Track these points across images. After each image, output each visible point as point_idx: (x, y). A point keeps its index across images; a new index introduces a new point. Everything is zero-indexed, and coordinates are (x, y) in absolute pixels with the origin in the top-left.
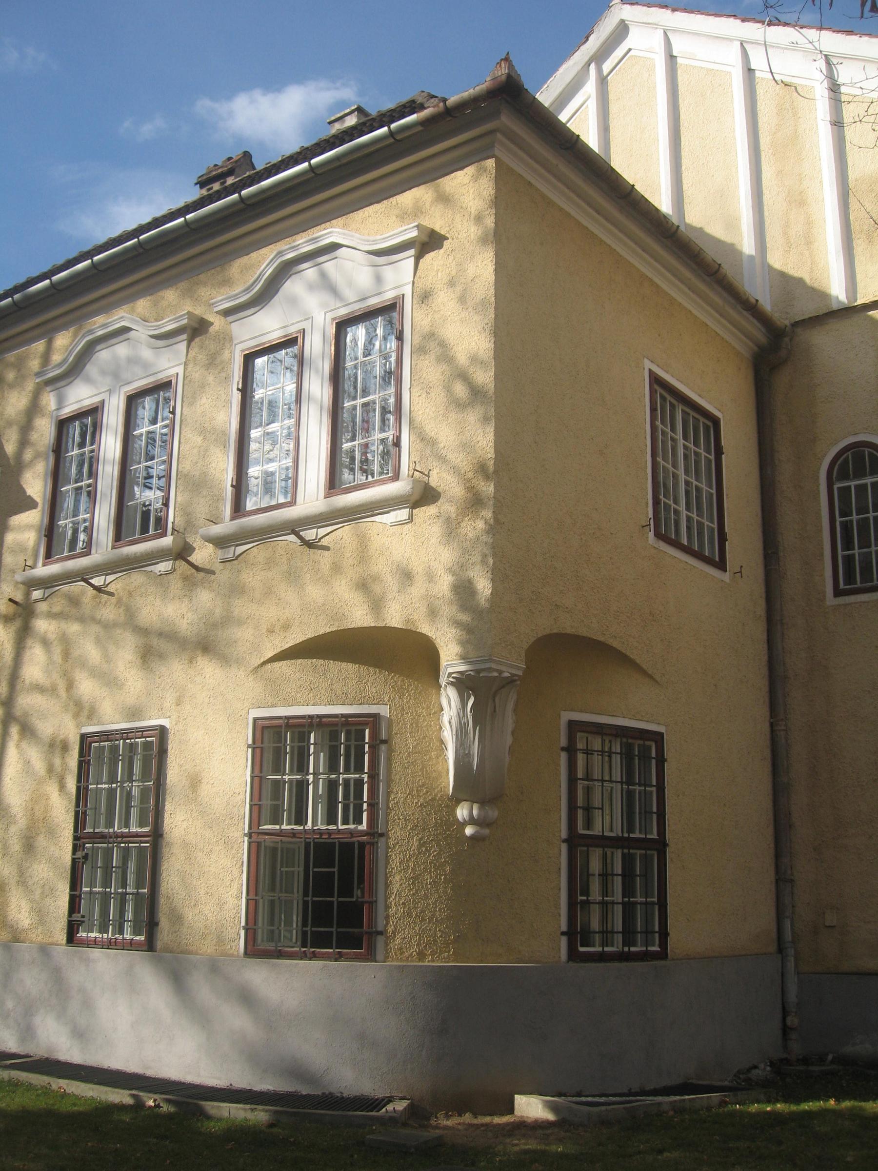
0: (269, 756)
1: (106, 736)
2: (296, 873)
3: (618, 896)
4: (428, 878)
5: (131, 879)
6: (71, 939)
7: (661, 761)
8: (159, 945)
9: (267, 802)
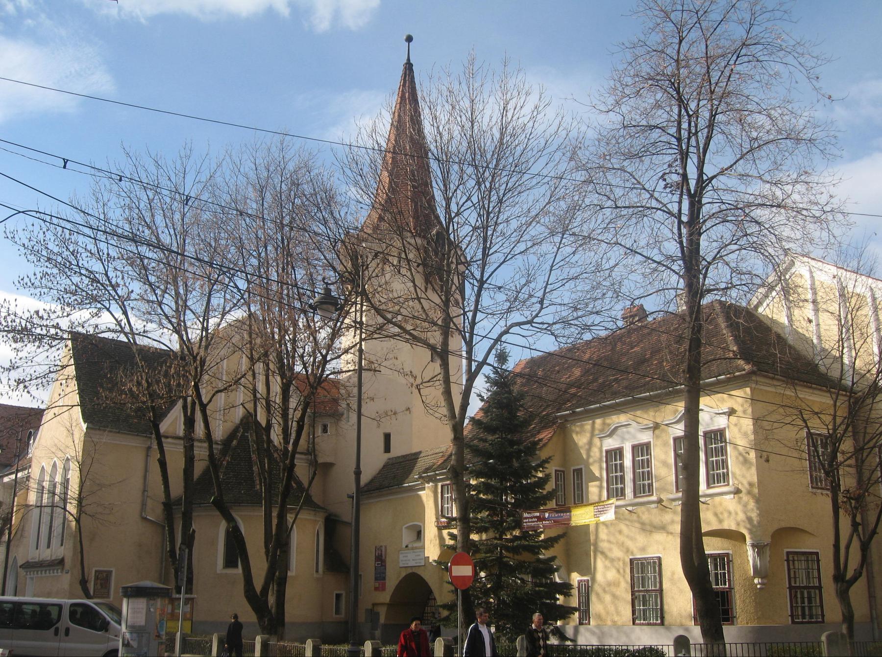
2: (55, 542)
3: (806, 604)
4: (748, 601)
6: (634, 623)
7: (818, 561)
8: (666, 623)
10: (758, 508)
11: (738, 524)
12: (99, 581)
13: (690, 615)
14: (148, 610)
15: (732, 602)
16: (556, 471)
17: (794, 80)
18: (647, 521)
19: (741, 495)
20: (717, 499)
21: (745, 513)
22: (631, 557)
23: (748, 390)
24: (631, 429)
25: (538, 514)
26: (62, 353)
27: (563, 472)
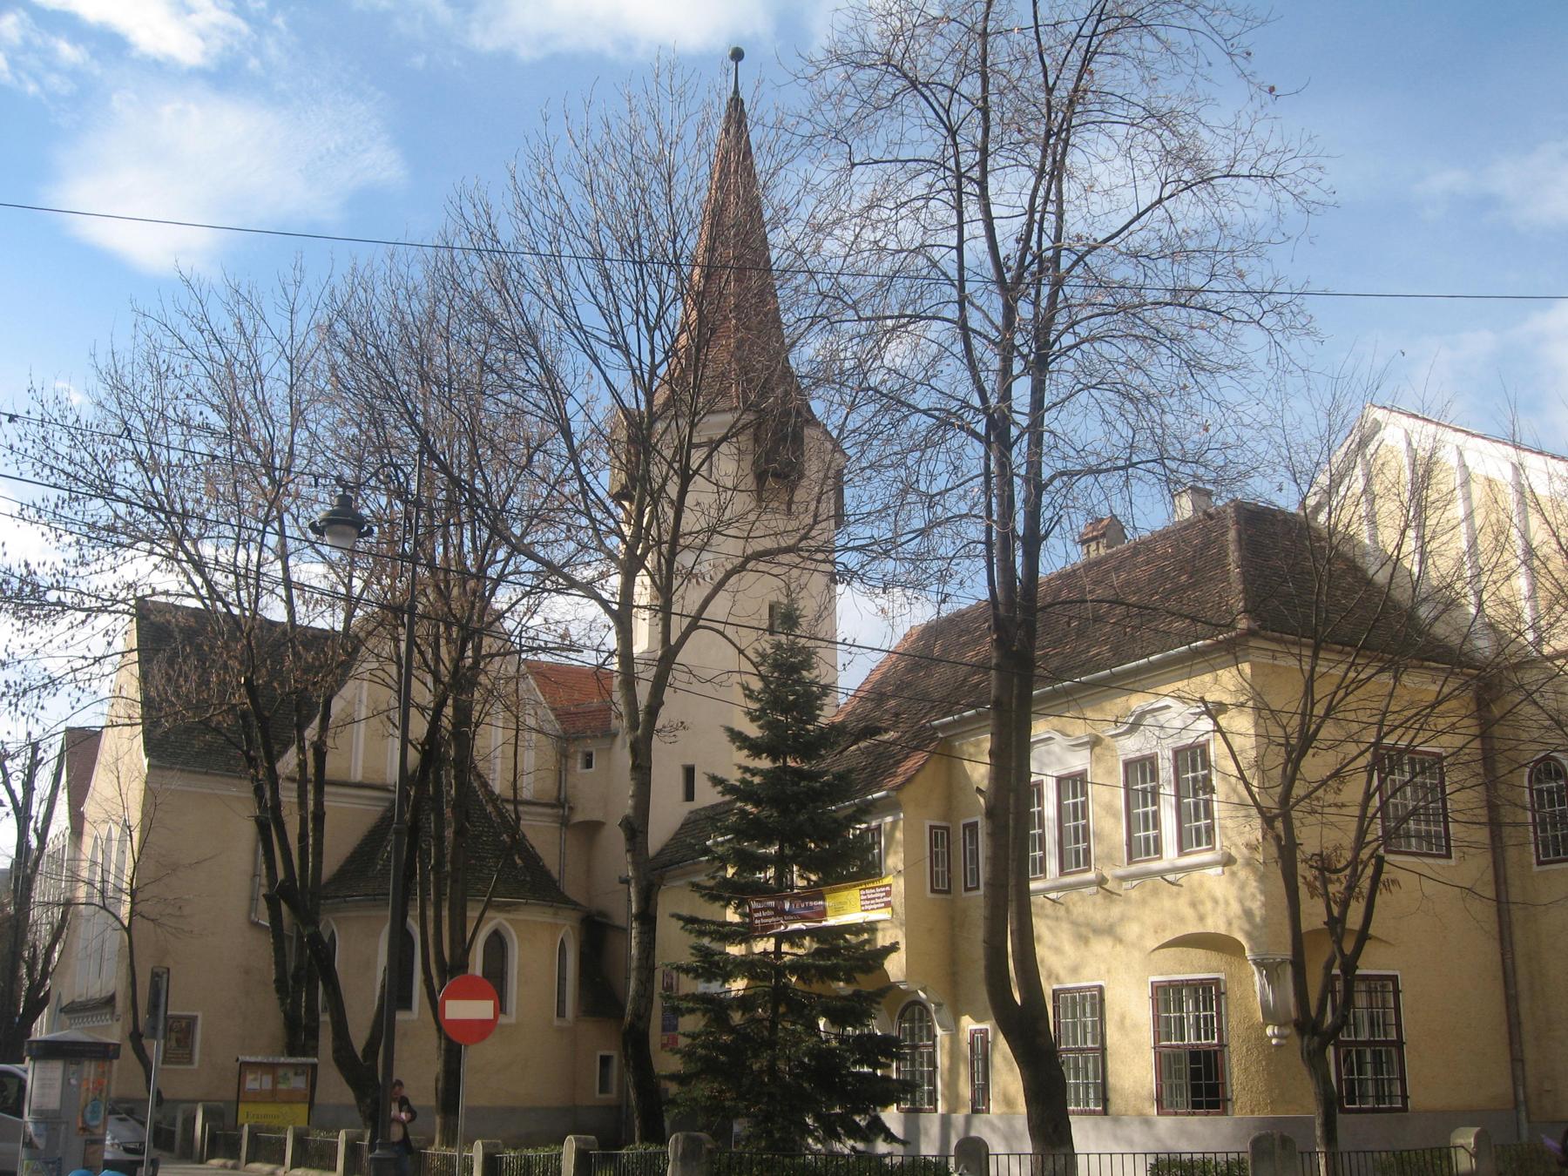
0: (1161, 1005)
1: (1068, 990)
5: (1091, 1074)
7: (1397, 992)
8: (1112, 1109)
9: (1163, 1029)
10: (1262, 892)
11: (1230, 924)
12: (173, 1036)
13: (1145, 1093)
14: (66, 1082)
15: (1223, 1071)
16: (932, 827)
17: (1202, 61)
18: (1081, 919)
19: (1234, 868)
20: (1196, 875)
21: (1241, 901)
22: (1056, 987)
23: (1246, 668)
24: (1055, 747)
25: (772, 903)
26: (123, 632)
27: (947, 829)
